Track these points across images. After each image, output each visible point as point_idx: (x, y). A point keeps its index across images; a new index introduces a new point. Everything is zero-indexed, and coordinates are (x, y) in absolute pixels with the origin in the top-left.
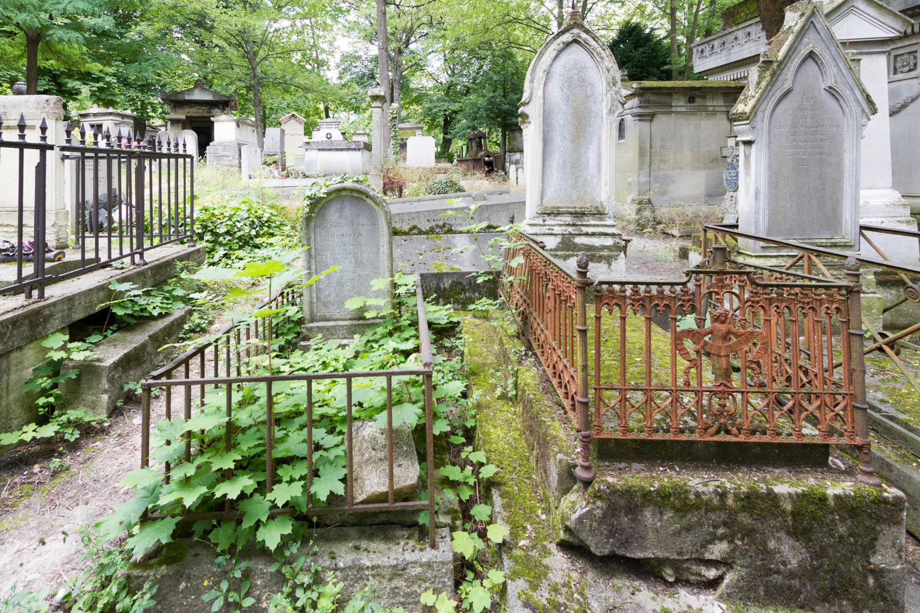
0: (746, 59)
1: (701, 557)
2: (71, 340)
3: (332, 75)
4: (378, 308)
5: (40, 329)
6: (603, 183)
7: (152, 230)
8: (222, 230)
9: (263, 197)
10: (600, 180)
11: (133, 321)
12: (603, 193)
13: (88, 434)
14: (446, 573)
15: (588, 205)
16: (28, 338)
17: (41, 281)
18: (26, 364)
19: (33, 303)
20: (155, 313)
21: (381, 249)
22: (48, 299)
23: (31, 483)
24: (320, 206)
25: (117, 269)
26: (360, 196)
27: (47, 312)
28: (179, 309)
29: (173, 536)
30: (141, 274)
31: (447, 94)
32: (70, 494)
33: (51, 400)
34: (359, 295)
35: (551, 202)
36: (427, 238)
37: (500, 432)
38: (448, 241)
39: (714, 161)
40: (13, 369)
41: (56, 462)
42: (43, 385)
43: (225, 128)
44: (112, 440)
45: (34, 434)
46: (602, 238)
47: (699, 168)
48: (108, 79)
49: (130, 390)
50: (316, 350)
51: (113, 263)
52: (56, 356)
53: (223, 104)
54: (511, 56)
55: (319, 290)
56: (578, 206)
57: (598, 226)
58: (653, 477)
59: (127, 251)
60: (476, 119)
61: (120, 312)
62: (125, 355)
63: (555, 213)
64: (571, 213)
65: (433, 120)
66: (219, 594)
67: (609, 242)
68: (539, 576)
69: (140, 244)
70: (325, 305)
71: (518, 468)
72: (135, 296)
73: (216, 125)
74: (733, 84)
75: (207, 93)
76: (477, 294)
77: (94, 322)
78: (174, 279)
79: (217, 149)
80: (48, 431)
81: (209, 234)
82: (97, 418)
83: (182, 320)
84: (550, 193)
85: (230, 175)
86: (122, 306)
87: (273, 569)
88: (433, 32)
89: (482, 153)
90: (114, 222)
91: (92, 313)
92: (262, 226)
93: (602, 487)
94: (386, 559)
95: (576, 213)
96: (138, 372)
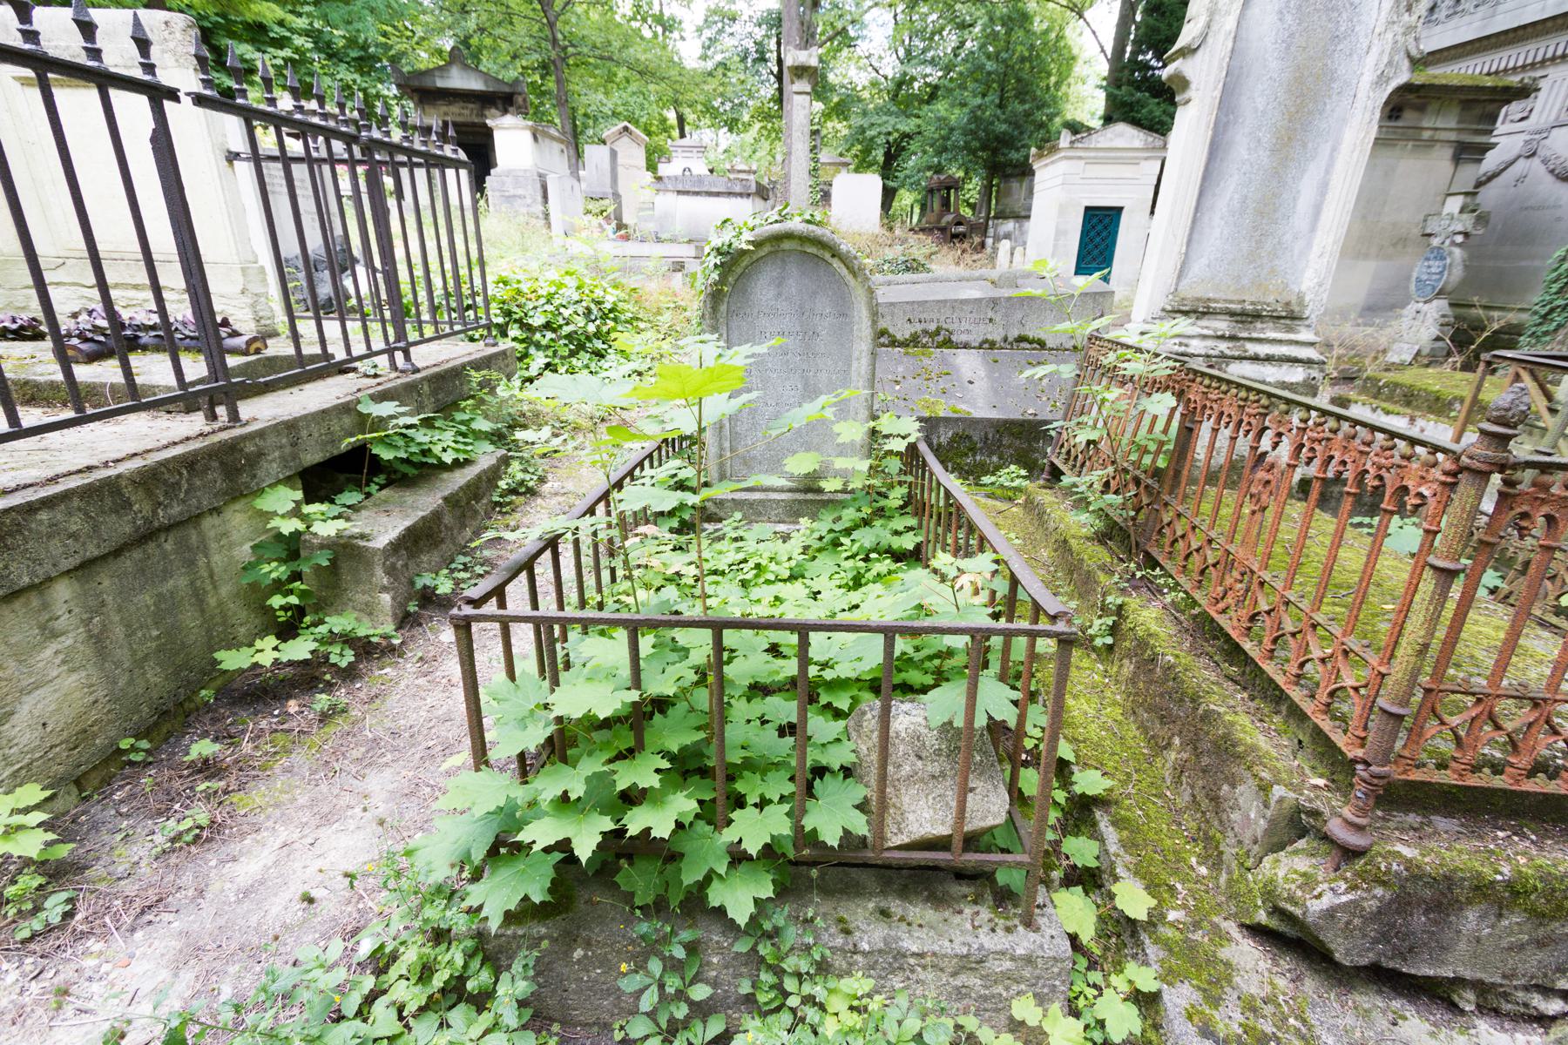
0: (1524, 27)
1: (1549, 985)
2: (309, 500)
3: (688, 52)
4: (845, 475)
5: (244, 478)
6: (1316, 249)
7: (418, 314)
8: (537, 320)
9: (596, 268)
10: (1309, 245)
11: (412, 471)
12: (1309, 273)
13: (368, 653)
14: (1059, 974)
15: (1270, 299)
16: (225, 493)
17: (222, 393)
18: (235, 536)
19: (221, 429)
20: (448, 458)
21: (855, 365)
22: (247, 423)
23: (290, 731)
24: (739, 270)
25: (367, 376)
26: (820, 253)
27: (250, 448)
28: (486, 456)
29: (550, 891)
30: (411, 388)
31: (895, 98)
32: (356, 754)
33: (294, 600)
34: (808, 450)
35: (1196, 287)
36: (907, 354)
37: (1085, 707)
38: (944, 361)
39: (1401, 242)
40: (213, 546)
41: (322, 701)
42: (274, 575)
43: (511, 138)
44: (410, 666)
45: (276, 654)
46: (1286, 366)
47: (1366, 256)
48: (299, 41)
49: (425, 587)
50: (736, 540)
51: (357, 364)
52: (288, 526)
53: (504, 99)
55: (735, 436)
56: (1250, 299)
57: (1280, 342)
58: (1492, 852)
59: (378, 344)
60: (945, 149)
61: (386, 455)
62: (408, 529)
63: (1199, 311)
64: (1232, 314)
65: (867, 151)
66: (648, 981)
67: (1297, 375)
68: (1218, 981)
69: (401, 334)
71: (1135, 776)
72: (408, 427)
73: (497, 135)
74: (1489, 82)
75: (473, 75)
76: (995, 459)
77: (342, 470)
78: (470, 402)
79: (503, 183)
80: (300, 649)
81: (516, 326)
82: (379, 631)
83: (493, 475)
84: (1197, 269)
85: (534, 222)
86: (385, 441)
87: (742, 946)
89: (949, 218)
90: (348, 297)
91: (336, 452)
92: (604, 317)
93: (1395, 867)
94: (947, 944)
95: (1243, 314)
96: (435, 557)
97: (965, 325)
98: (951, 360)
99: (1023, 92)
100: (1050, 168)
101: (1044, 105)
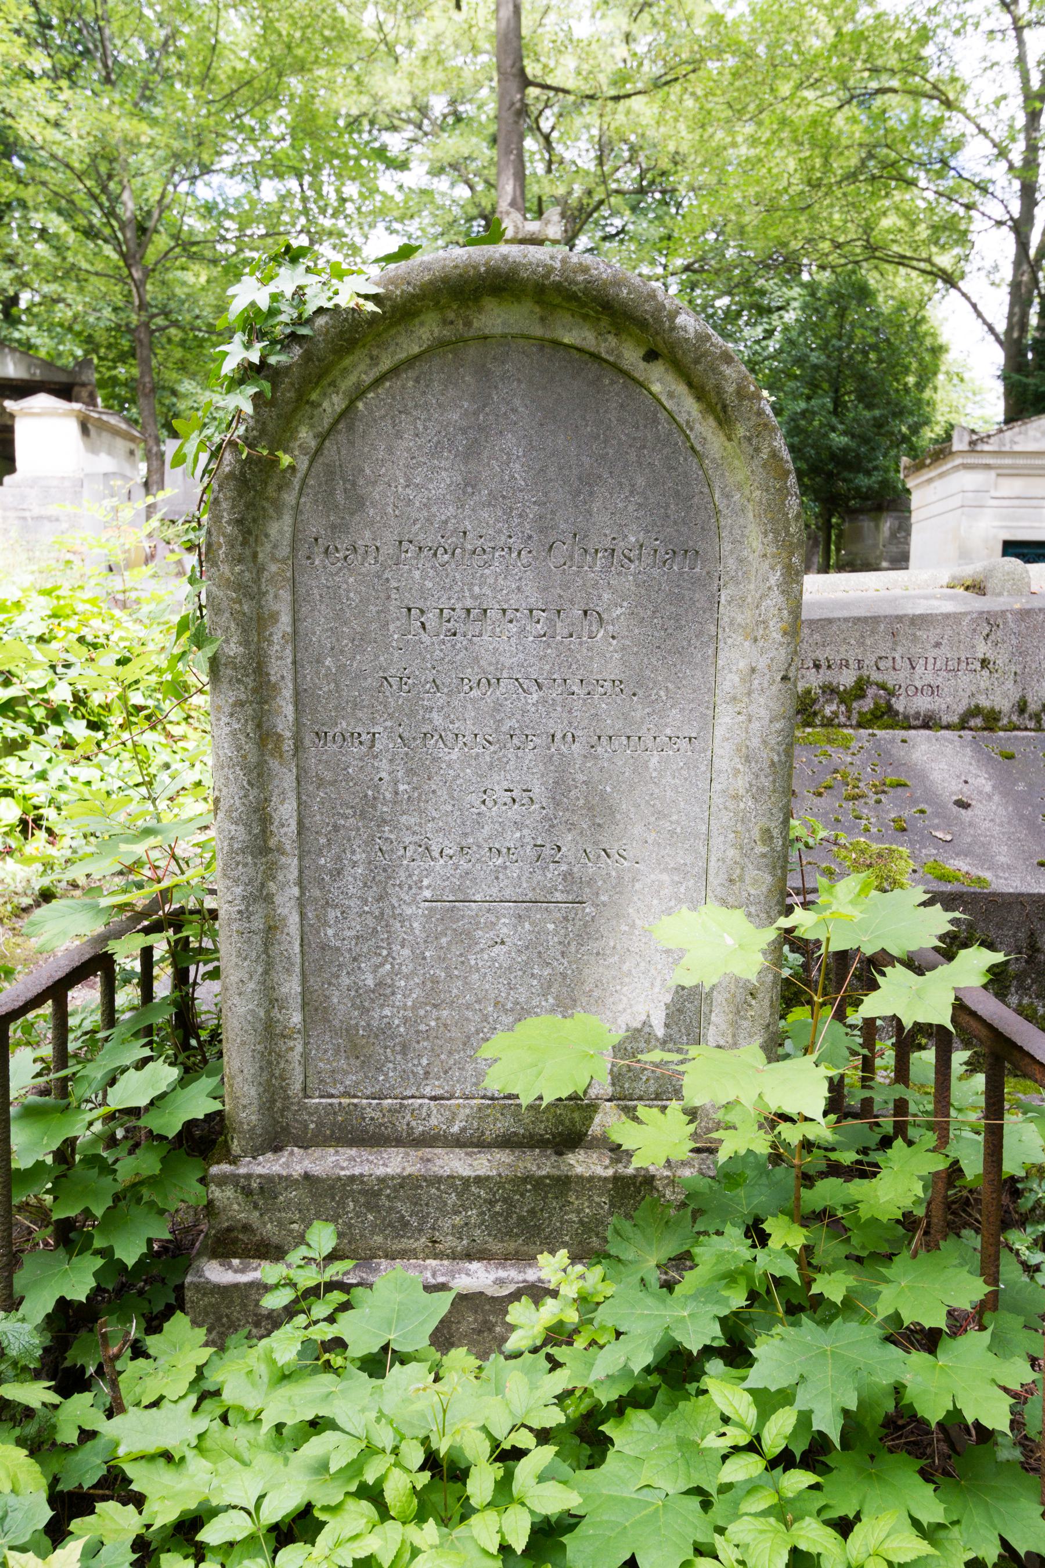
26: (606, 346)
38: (882, 755)
54: (863, 293)
70: (357, 1048)
88: (642, 226)
97: (923, 675)
98: (899, 752)
99: (868, 395)
100: (937, 484)
101: (900, 413)
